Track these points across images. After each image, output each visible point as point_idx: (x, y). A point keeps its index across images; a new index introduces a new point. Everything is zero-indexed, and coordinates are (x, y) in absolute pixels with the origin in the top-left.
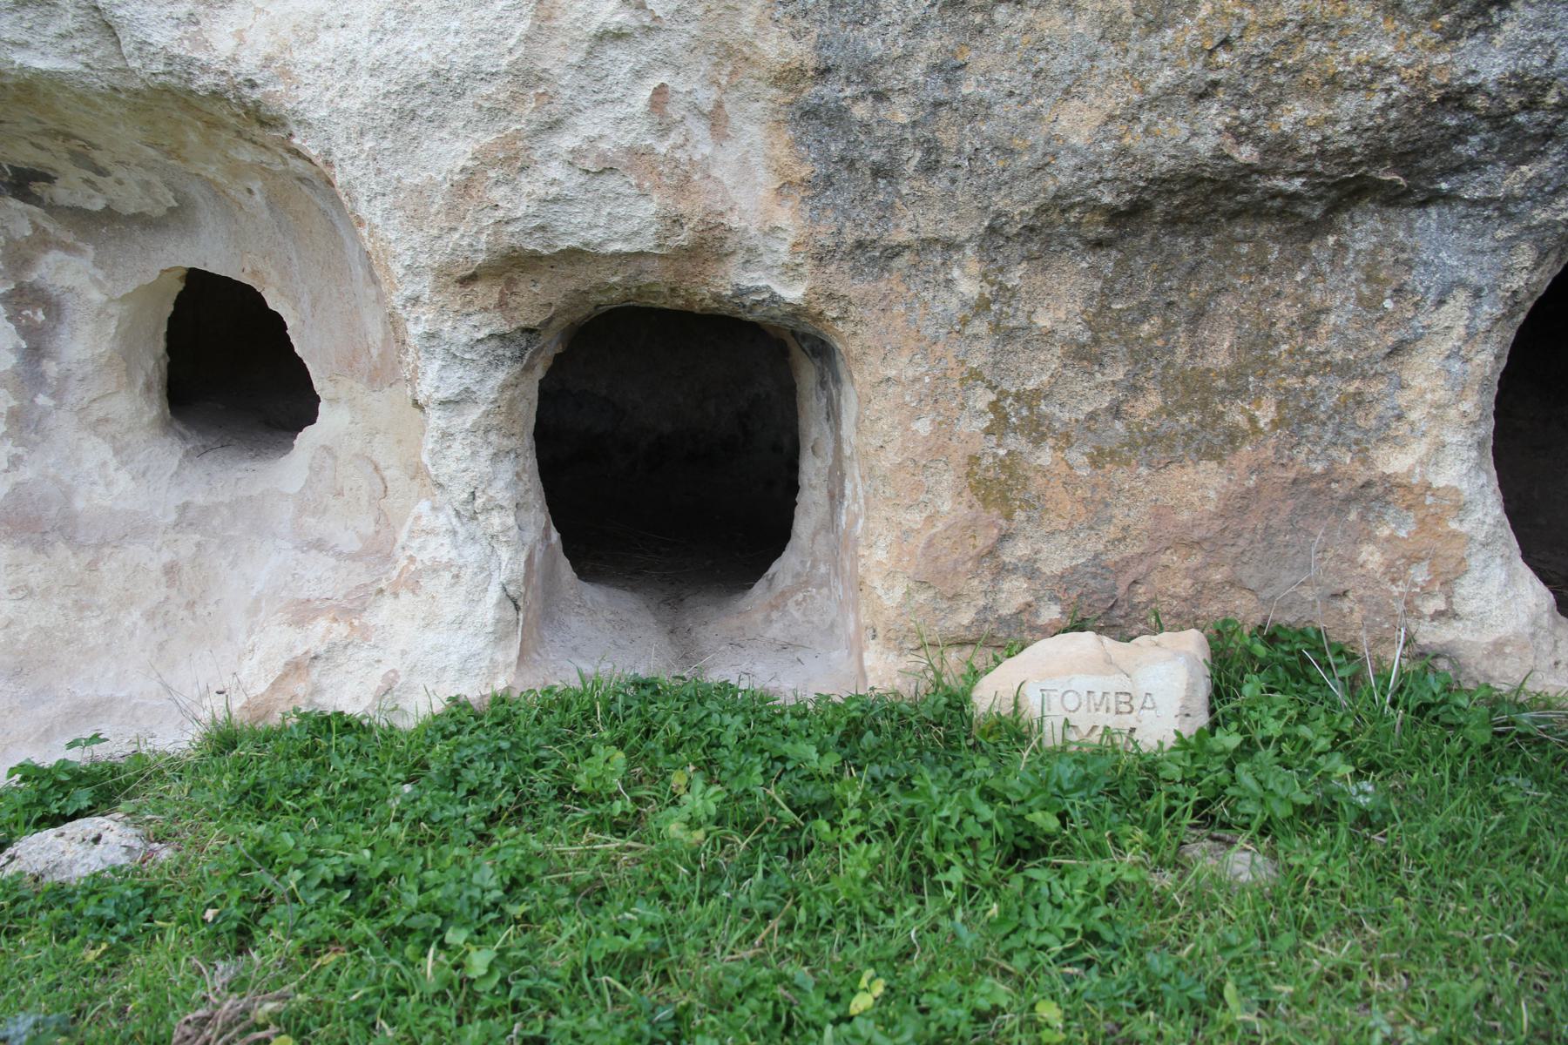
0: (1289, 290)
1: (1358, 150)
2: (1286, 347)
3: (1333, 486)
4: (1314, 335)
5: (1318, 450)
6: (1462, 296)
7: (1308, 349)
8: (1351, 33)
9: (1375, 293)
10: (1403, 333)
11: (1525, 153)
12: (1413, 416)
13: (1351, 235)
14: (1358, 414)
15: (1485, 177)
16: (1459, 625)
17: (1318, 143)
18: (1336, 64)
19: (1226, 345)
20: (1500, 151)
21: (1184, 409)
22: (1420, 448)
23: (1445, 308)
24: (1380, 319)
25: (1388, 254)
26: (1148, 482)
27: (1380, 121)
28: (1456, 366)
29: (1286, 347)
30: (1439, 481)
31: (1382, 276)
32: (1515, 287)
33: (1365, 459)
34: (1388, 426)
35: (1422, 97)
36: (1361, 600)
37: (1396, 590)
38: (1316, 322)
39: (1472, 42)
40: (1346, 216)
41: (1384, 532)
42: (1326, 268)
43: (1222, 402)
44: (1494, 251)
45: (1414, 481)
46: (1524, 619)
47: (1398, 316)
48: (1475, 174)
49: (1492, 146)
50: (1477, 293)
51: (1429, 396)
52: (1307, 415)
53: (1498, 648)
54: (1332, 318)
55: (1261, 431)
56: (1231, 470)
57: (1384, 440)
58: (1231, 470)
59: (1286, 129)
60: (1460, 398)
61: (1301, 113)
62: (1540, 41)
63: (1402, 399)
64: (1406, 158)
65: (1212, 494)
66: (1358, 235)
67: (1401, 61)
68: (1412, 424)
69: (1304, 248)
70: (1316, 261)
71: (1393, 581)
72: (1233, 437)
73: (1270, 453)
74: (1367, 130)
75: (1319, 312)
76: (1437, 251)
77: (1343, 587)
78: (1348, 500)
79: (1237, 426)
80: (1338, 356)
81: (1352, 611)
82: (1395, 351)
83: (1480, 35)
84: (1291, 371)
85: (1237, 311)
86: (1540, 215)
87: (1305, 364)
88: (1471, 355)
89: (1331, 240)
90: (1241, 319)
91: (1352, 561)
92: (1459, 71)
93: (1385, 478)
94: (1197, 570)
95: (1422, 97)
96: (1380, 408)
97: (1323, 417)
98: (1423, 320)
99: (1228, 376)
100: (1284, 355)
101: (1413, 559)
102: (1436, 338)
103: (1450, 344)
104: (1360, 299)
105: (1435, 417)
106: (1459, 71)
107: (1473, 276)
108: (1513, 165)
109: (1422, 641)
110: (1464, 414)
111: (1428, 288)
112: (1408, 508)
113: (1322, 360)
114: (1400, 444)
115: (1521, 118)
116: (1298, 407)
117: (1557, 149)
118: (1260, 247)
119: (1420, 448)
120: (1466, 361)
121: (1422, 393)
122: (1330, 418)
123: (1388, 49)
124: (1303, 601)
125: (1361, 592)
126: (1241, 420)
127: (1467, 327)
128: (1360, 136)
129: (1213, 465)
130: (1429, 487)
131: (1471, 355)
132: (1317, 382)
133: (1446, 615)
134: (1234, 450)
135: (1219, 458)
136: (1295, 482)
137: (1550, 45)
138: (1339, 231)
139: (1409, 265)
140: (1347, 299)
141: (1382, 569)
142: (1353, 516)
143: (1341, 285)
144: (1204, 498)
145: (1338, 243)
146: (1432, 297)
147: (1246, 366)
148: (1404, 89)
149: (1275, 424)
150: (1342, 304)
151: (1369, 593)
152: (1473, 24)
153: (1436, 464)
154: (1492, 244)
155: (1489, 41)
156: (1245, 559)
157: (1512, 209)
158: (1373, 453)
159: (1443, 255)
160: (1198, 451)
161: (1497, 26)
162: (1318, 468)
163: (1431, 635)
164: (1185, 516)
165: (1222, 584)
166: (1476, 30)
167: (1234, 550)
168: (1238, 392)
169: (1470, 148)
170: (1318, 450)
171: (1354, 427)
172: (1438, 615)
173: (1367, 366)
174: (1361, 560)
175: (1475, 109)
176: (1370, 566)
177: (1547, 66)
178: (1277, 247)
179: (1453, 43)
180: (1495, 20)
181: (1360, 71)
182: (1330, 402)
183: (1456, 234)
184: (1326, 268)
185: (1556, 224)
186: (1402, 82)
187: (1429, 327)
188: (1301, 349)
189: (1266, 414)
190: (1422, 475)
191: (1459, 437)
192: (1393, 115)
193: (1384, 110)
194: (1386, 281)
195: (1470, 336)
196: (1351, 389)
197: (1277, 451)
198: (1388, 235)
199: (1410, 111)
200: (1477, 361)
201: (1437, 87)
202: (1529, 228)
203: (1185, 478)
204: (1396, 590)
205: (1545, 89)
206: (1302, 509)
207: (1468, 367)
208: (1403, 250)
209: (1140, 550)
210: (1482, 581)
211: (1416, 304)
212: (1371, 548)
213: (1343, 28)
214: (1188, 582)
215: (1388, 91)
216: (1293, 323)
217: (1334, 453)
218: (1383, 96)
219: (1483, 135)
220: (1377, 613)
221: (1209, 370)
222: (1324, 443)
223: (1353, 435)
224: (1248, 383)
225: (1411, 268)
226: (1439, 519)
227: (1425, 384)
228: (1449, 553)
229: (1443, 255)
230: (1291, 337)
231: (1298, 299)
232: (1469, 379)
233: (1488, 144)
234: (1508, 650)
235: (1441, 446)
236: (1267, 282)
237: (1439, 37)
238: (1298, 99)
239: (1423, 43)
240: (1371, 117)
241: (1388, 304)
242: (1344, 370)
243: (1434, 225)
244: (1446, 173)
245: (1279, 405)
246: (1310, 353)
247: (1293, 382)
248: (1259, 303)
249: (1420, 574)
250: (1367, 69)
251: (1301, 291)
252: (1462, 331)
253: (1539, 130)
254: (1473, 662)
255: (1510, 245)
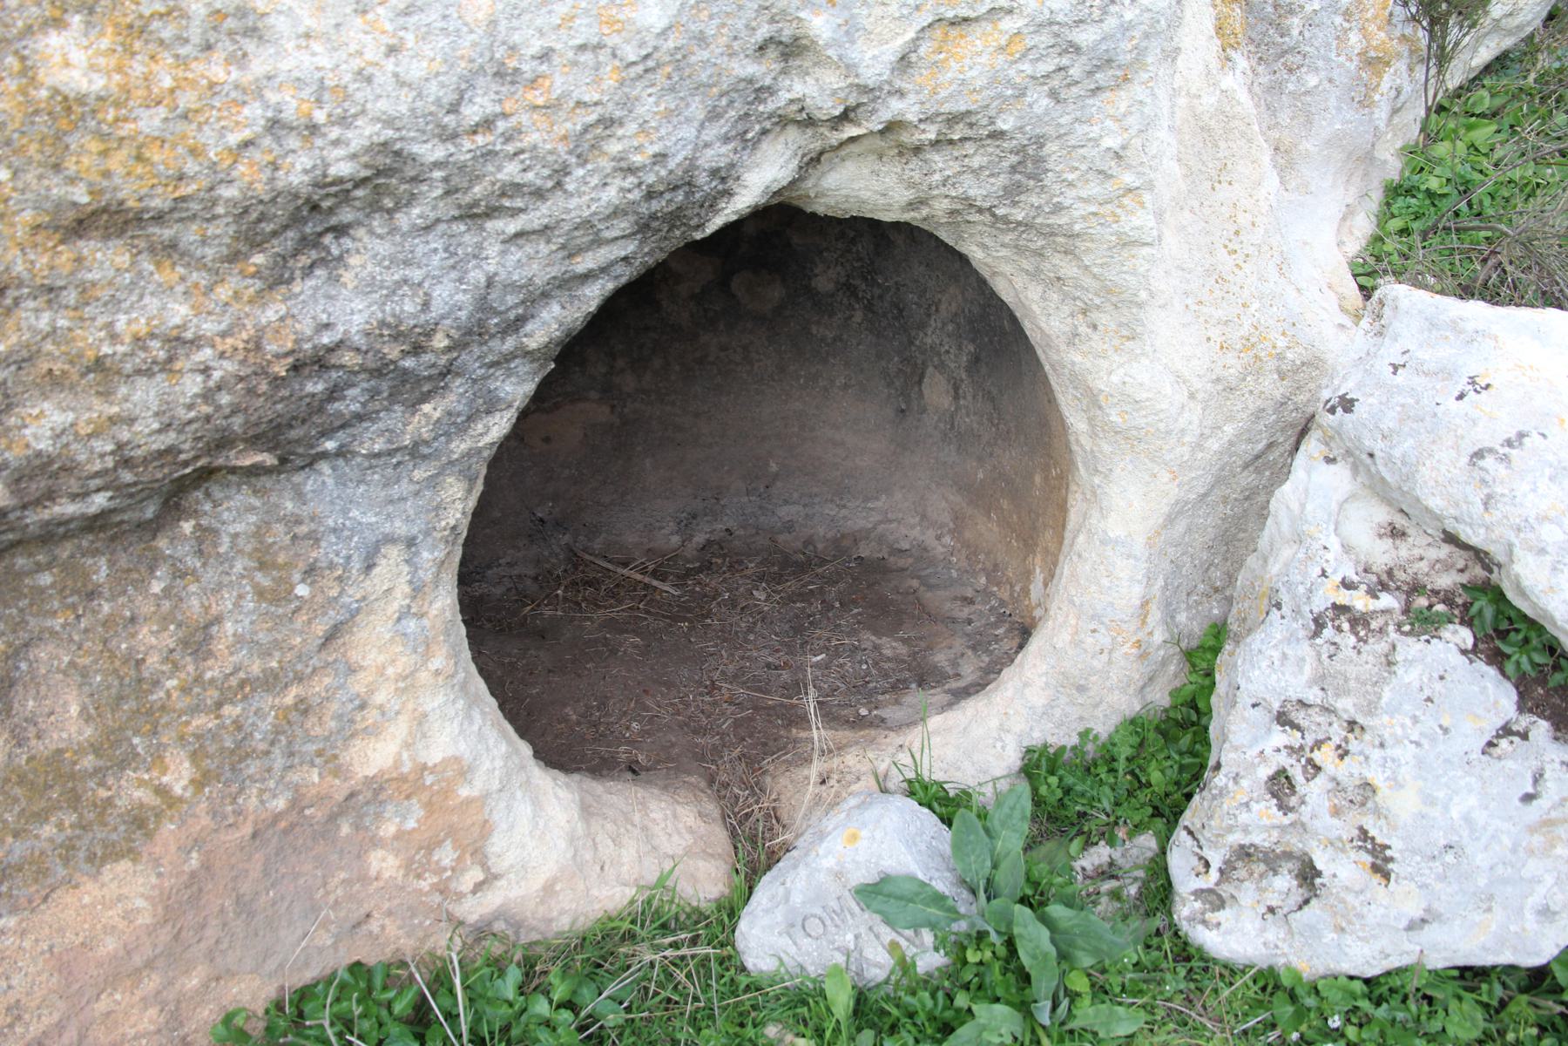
0: (147, 608)
1: (186, 446)
2: (174, 682)
3: (307, 812)
4: (210, 654)
5: (272, 784)
6: (394, 553)
7: (209, 675)
8: (105, 294)
9: (278, 581)
10: (333, 616)
11: (422, 394)
12: (380, 698)
13: (217, 516)
14: (309, 725)
15: (381, 425)
16: (502, 883)
17: (112, 453)
18: (92, 340)
19: (74, 710)
20: (391, 395)
21: (42, 817)
22: (400, 729)
23: (376, 571)
24: (298, 609)
25: (279, 531)
26: (23, 933)
27: (206, 409)
28: (411, 625)
29: (174, 682)
30: (434, 756)
31: (281, 559)
32: (452, 522)
33: (338, 771)
34: (352, 721)
35: (262, 372)
36: (390, 913)
37: (424, 885)
38: (208, 638)
39: (311, 283)
40: (199, 494)
41: (389, 829)
42: (193, 562)
43: (102, 784)
44: (417, 494)
45: (405, 770)
46: (562, 844)
47: (319, 599)
48: (365, 425)
49: (379, 393)
50: (411, 542)
51: (390, 671)
52: (240, 754)
53: (549, 889)
54: (229, 627)
55: (181, 800)
56: (157, 862)
57: (353, 736)
58: (157, 862)
59: (44, 445)
60: (427, 656)
61: (59, 418)
62: (405, 281)
63: (358, 685)
64: (269, 435)
65: (140, 903)
66: (226, 515)
67: (209, 327)
68: (381, 707)
69: (150, 549)
70: (174, 562)
71: (419, 876)
72: (140, 821)
73: (206, 820)
74: (190, 422)
75: (206, 627)
76: (345, 512)
77: (363, 911)
78: (333, 818)
79: (141, 805)
80: (256, 668)
81: (383, 927)
82: (330, 638)
83: (318, 272)
84: (195, 710)
85: (72, 664)
86: (459, 447)
87: (213, 695)
88: (425, 609)
89: (187, 527)
90: (85, 673)
91: (364, 879)
92: (307, 327)
93: (369, 781)
94: (158, 993)
95: (262, 372)
96: (334, 707)
97: (262, 746)
98: (353, 593)
99: (96, 750)
100: (175, 695)
101: (431, 846)
102: (376, 605)
103: (396, 606)
104: (260, 593)
105: (405, 689)
106: (307, 327)
107: (400, 528)
108: (413, 406)
109: (472, 918)
110: (437, 673)
111: (349, 558)
112: (408, 797)
113: (234, 682)
114: (374, 732)
115: (409, 363)
116: (222, 749)
117: (458, 381)
118: (69, 568)
119: (400, 729)
120: (421, 616)
121: (381, 671)
122: (272, 743)
123: (179, 312)
124: (320, 950)
125: (387, 905)
126: (142, 795)
127: (410, 582)
128: (180, 432)
129: (124, 865)
130: (424, 767)
131: (425, 609)
132: (238, 710)
133: (490, 879)
134: (149, 835)
135: (132, 854)
136: (254, 835)
137: (420, 285)
138: (196, 514)
139: (315, 538)
140: (240, 597)
141: (402, 872)
142: (345, 829)
143: (226, 579)
144: (128, 916)
145: (198, 527)
146: (356, 565)
147: (121, 729)
148: (230, 366)
149: (198, 784)
150: (236, 605)
151: (396, 902)
152: (304, 260)
153: (424, 736)
154: (413, 488)
155: (335, 280)
156: (224, 946)
157: (425, 450)
158: (345, 758)
159: (355, 513)
160: (91, 858)
161: (340, 258)
162: (280, 804)
163: (473, 910)
164: (110, 945)
165: (206, 985)
166: (312, 266)
167: (203, 945)
168: (129, 760)
169: (351, 403)
170: (272, 784)
171: (309, 739)
172: (478, 887)
173: (299, 667)
174: (373, 873)
175: (342, 367)
176: (386, 875)
177: (423, 311)
178: (103, 562)
179: (283, 289)
180: (335, 251)
181: (145, 349)
182: (266, 725)
183: (362, 488)
184: (193, 562)
185: (479, 451)
186: (222, 355)
187: (364, 598)
188: (198, 679)
189: (179, 775)
190: (413, 759)
191: (440, 699)
192: (225, 399)
193: (207, 395)
194: (288, 566)
195: (417, 590)
196: (289, 699)
197: (214, 813)
198: (272, 509)
199: (251, 392)
200: (433, 612)
201: (277, 356)
202: (451, 463)
203: (87, 900)
204: (424, 885)
205: (429, 334)
206: (277, 854)
207: (425, 622)
208: (299, 522)
209: (56, 1017)
210: (511, 827)
211: (340, 579)
212: (380, 853)
213: (85, 289)
214: (152, 1012)
215: (206, 371)
216: (172, 651)
217: (294, 777)
218: (199, 378)
219: (365, 385)
220: (413, 916)
221: (60, 752)
222: (277, 772)
223: (311, 748)
224: (133, 747)
225: (317, 540)
226: (447, 792)
227: (381, 659)
228: (469, 822)
229: (355, 513)
230: (176, 667)
231: (165, 621)
232: (430, 634)
233: (374, 394)
234: (558, 888)
235: (421, 719)
236: (106, 608)
237: (259, 284)
238: (46, 398)
239: (237, 295)
240: (190, 407)
241: (302, 590)
242: (271, 682)
243: (330, 482)
244: (326, 433)
245: (194, 757)
246: (212, 680)
247: (202, 722)
248: (105, 642)
249: (446, 855)
250: (155, 344)
251: (167, 605)
252: (407, 589)
253: (434, 371)
254: (528, 914)
255: (433, 482)
